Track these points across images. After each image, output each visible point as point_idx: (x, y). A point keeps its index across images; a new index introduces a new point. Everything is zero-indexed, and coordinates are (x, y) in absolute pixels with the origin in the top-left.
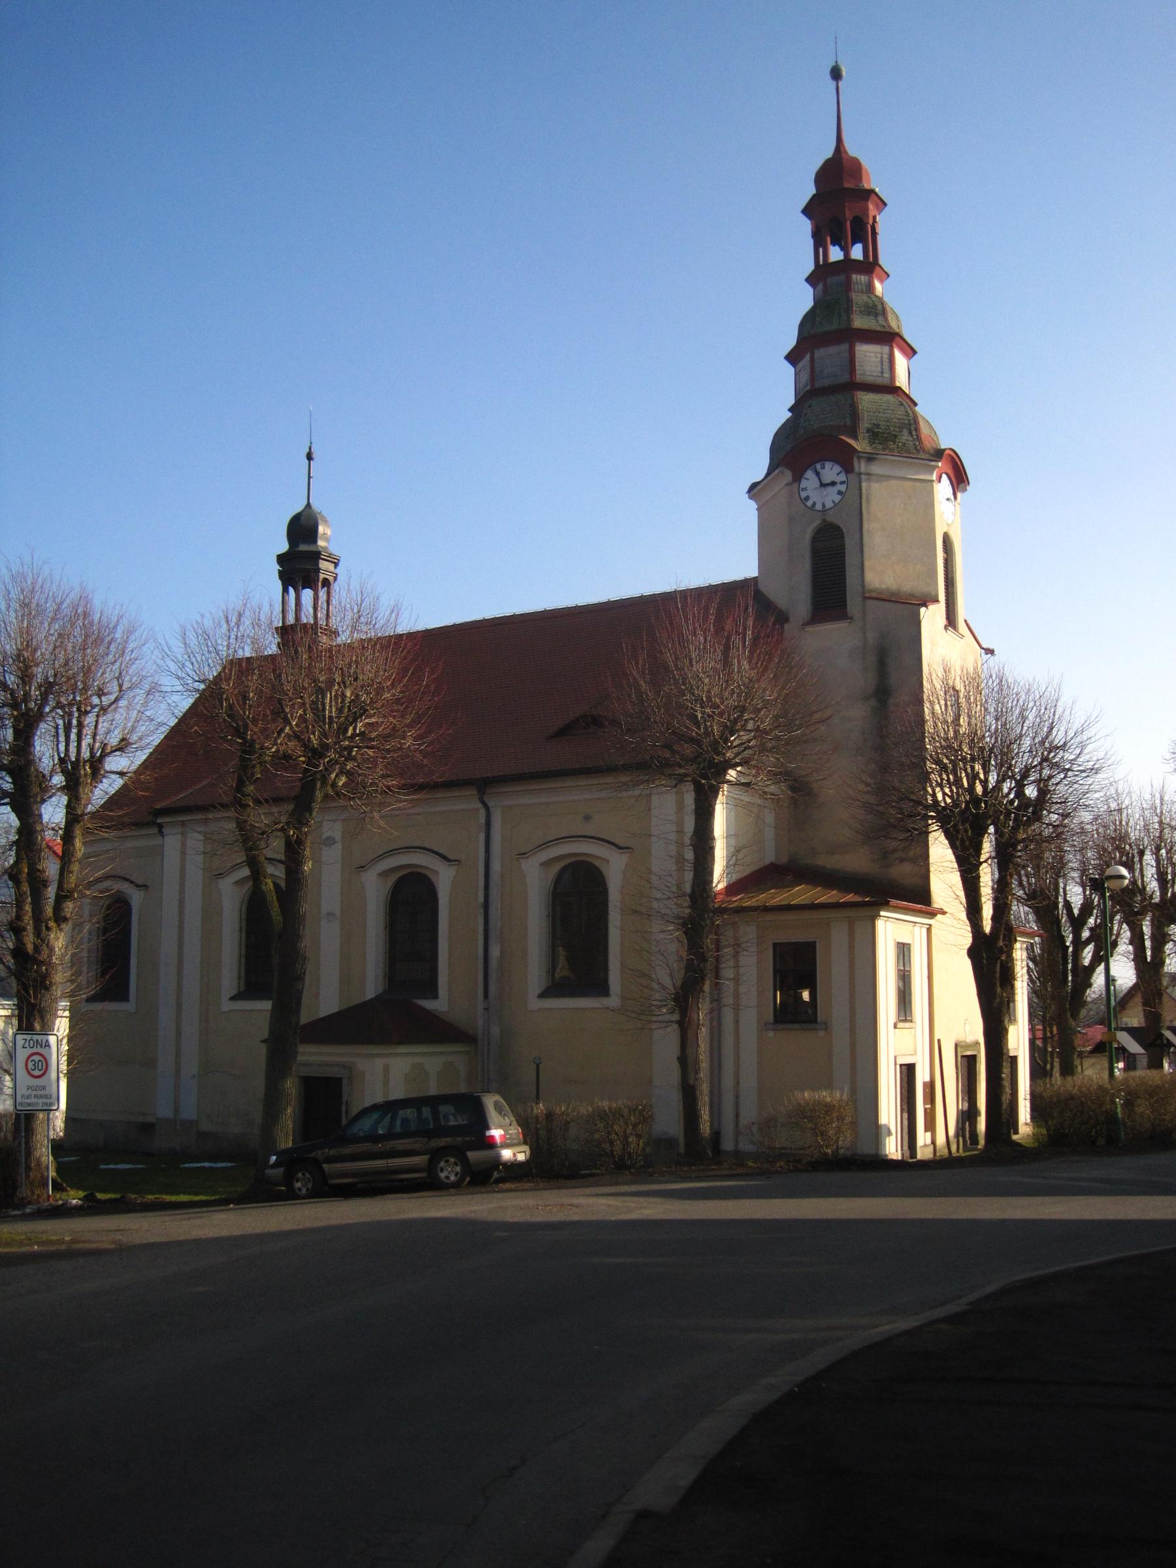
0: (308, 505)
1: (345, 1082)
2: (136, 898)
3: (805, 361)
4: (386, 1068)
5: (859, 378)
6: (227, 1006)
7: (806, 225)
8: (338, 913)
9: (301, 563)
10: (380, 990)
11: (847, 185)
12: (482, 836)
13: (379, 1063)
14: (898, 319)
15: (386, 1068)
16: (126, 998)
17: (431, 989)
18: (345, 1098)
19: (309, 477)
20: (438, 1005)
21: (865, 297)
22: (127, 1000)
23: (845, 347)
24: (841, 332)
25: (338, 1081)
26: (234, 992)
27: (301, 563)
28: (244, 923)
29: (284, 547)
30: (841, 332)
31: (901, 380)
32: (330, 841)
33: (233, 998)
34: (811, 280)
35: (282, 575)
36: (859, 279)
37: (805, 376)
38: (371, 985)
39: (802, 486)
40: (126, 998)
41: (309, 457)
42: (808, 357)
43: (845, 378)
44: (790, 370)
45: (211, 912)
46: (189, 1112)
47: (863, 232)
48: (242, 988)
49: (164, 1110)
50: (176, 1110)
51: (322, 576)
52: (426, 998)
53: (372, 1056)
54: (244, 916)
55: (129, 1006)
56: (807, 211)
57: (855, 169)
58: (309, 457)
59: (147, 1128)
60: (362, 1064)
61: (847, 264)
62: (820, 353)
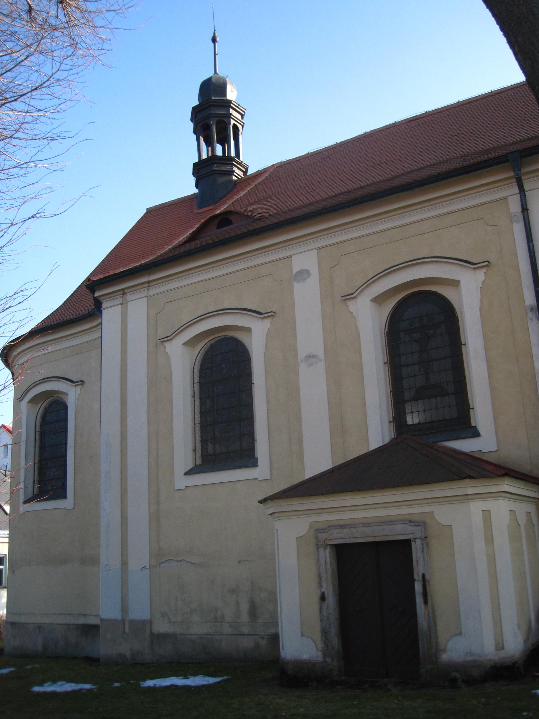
1: (416, 547)
2: (72, 396)
4: (487, 514)
6: (182, 482)
8: (321, 354)
9: (213, 115)
10: (387, 440)
12: (519, 229)
13: (476, 508)
15: (487, 514)
16: (63, 496)
17: (465, 426)
18: (419, 570)
19: (215, 55)
20: (484, 444)
22: (65, 497)
25: (405, 545)
26: (190, 466)
27: (213, 115)
28: (197, 386)
29: (196, 102)
32: (304, 274)
33: (186, 474)
38: (377, 432)
40: (63, 496)
41: (214, 40)
45: (158, 379)
46: (140, 611)
48: (199, 462)
49: (108, 609)
50: (124, 609)
51: (232, 122)
52: (458, 438)
53: (466, 498)
54: (197, 380)
55: (67, 503)
58: (214, 40)
59: (90, 630)
60: (443, 514)
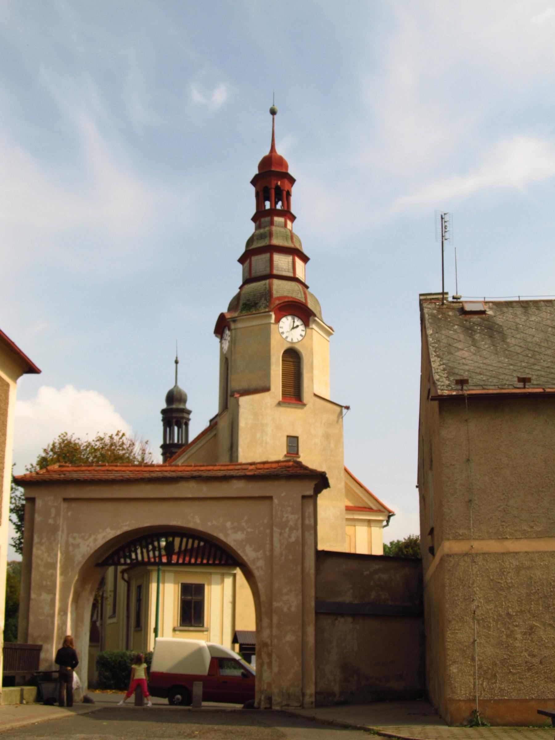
0: (176, 386)
3: (248, 262)
5: (275, 272)
7: (252, 190)
11: (273, 169)
14: (300, 242)
21: (283, 230)
23: (268, 255)
24: (267, 249)
29: (164, 406)
30: (267, 249)
31: (300, 274)
34: (254, 219)
35: (164, 420)
36: (278, 220)
37: (247, 270)
39: (300, 338)
41: (177, 362)
42: (248, 261)
43: (268, 271)
44: (240, 267)
47: (283, 195)
56: (254, 182)
57: (281, 162)
58: (177, 362)
61: (273, 212)
62: (254, 259)
